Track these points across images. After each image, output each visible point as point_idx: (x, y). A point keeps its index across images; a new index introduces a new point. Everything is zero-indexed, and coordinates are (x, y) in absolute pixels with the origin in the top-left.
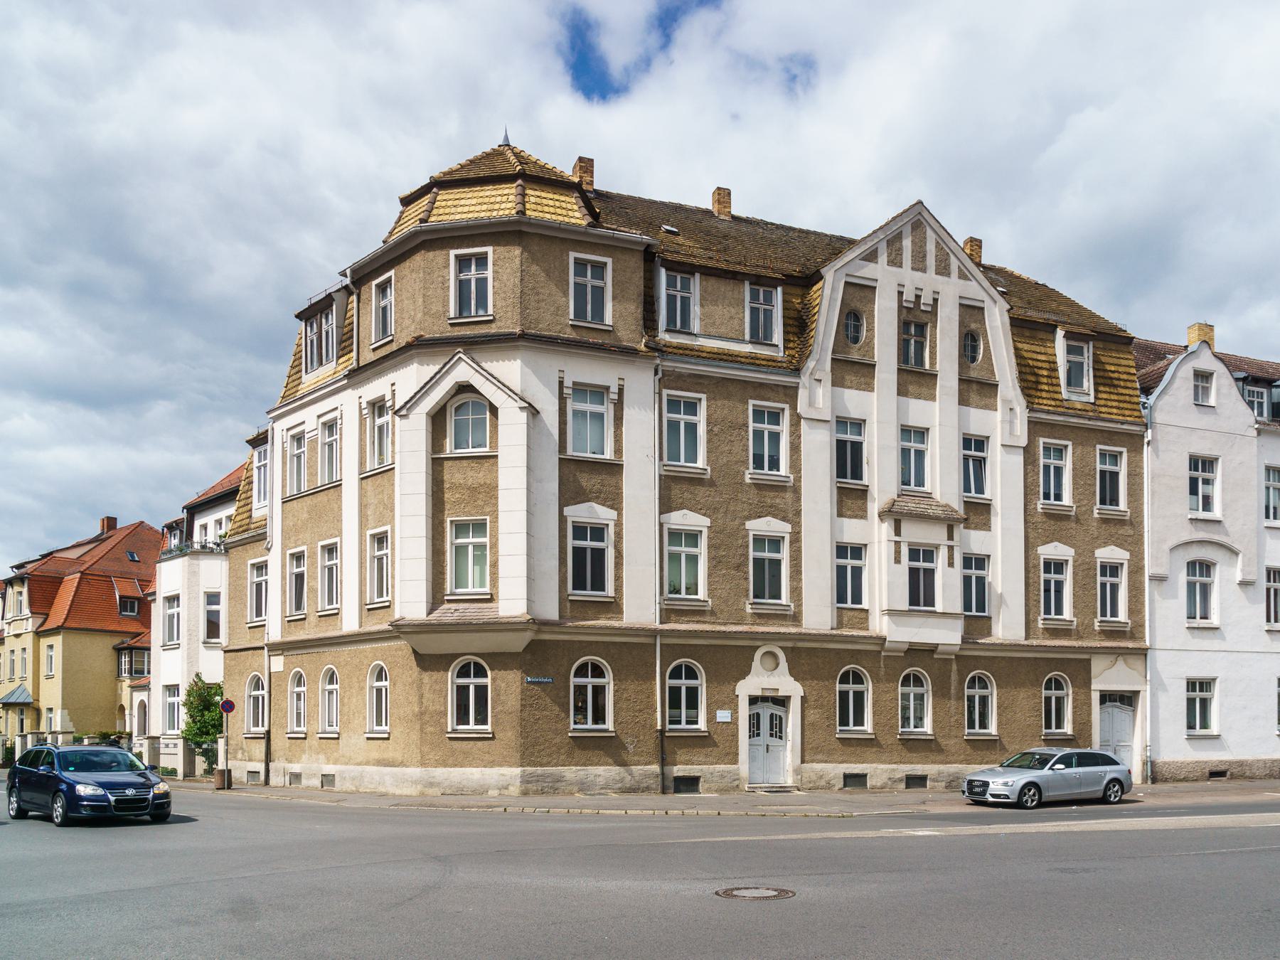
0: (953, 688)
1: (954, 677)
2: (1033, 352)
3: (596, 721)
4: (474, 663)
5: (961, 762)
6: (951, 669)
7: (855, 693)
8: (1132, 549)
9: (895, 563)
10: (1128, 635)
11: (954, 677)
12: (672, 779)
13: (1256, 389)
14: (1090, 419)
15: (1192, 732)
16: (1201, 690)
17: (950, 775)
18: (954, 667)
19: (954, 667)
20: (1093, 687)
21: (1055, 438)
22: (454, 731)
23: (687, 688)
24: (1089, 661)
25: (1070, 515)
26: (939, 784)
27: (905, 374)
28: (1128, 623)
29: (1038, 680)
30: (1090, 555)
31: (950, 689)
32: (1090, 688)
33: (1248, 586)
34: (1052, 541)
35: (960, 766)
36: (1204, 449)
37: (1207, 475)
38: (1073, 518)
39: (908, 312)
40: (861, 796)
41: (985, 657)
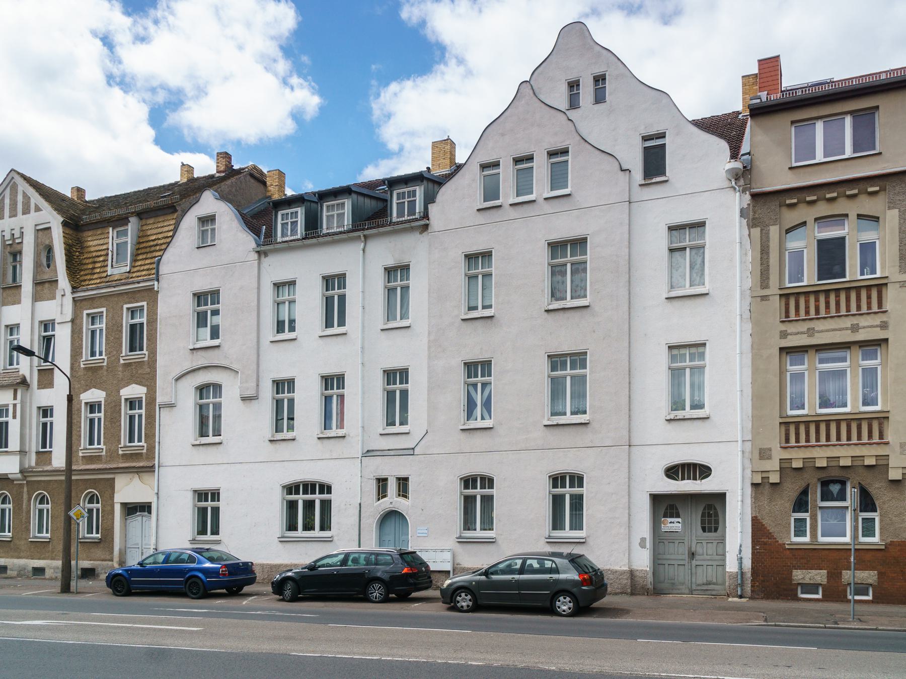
0: (24, 504)
1: (25, 496)
2: (99, 245)
3: (322, 528)
4: (577, 476)
5: (27, 558)
6: (23, 491)
7: (572, 497)
8: (149, 384)
9: (13, 418)
10: (144, 456)
11: (25, 496)
12: (31, 569)
13: (289, 211)
14: (114, 287)
15: (558, 533)
16: (572, 486)
17: (19, 567)
18: (25, 489)
19: (25, 489)
20: (115, 501)
21: (94, 308)
22: (84, 538)
23: (572, 496)
24: (114, 478)
25: (103, 366)
26: (14, 572)
27: (8, 290)
28: (144, 446)
29: (78, 497)
30: (117, 394)
31: (23, 505)
32: (114, 501)
33: (253, 401)
34: (90, 388)
35: (26, 560)
36: (203, 285)
37: (215, 307)
38: (105, 367)
39: (10, 247)
40: (788, 604)
41: (44, 481)
